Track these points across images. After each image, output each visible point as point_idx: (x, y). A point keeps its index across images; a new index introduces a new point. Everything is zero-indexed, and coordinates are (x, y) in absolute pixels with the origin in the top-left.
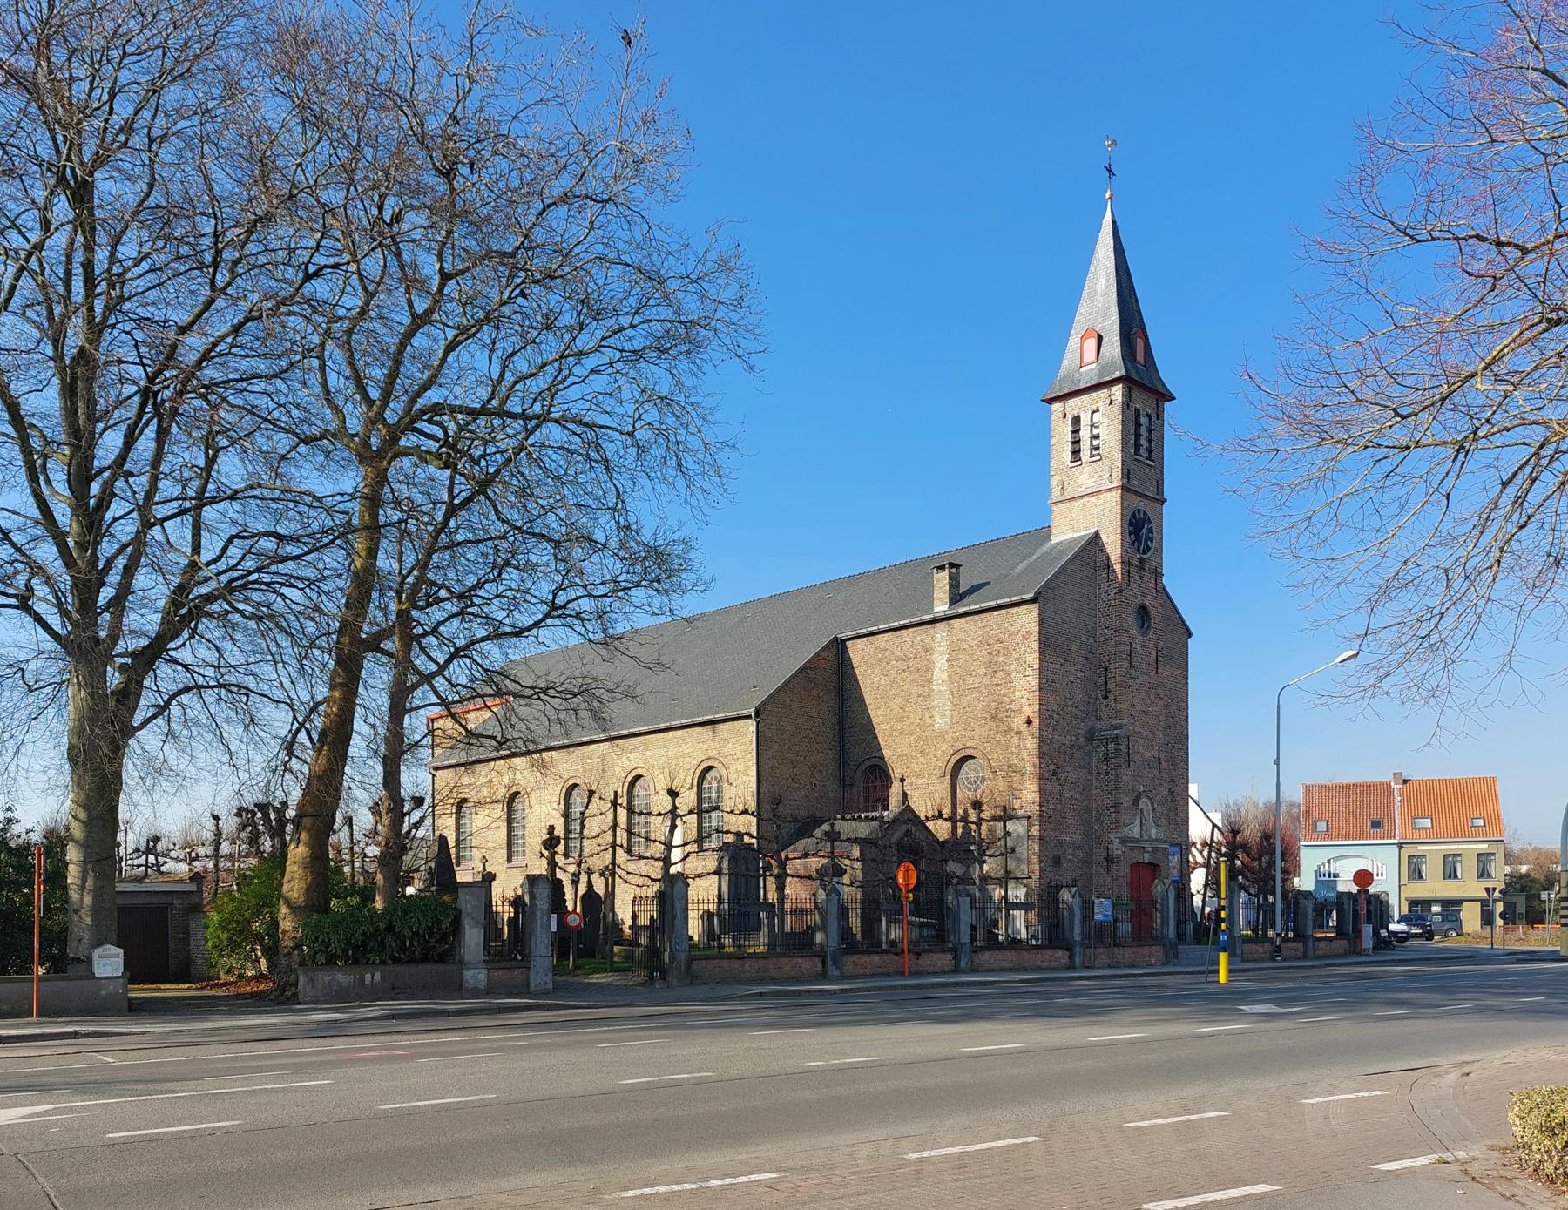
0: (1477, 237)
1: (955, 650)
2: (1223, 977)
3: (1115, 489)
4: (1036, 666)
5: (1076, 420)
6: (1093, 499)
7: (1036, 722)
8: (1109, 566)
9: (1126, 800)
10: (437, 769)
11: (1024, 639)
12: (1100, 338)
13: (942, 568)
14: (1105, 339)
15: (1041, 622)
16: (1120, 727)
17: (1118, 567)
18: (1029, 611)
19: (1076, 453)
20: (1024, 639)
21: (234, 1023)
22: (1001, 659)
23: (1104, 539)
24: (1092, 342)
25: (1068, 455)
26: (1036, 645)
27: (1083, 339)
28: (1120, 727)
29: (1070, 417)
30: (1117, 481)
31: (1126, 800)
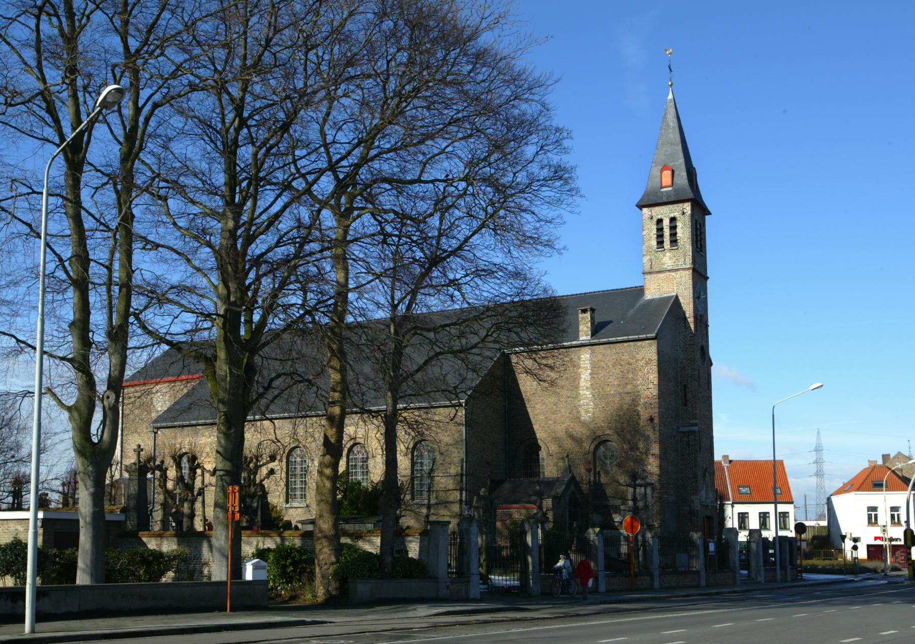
0: (53, 159)
1: (595, 368)
2: (82, 579)
3: (689, 269)
4: (656, 382)
5: (660, 221)
6: (673, 274)
7: (656, 421)
8: (685, 318)
9: (700, 473)
10: (158, 428)
11: (647, 364)
12: (673, 172)
13: (584, 311)
14: (676, 173)
15: (659, 353)
16: (695, 425)
17: (691, 320)
18: (650, 345)
19: (660, 243)
20: (647, 364)
21: (481, 634)
22: (630, 376)
23: (681, 300)
24: (668, 173)
25: (654, 243)
26: (655, 368)
27: (662, 171)
28: (695, 425)
29: (655, 220)
30: (689, 263)
31: (700, 473)
